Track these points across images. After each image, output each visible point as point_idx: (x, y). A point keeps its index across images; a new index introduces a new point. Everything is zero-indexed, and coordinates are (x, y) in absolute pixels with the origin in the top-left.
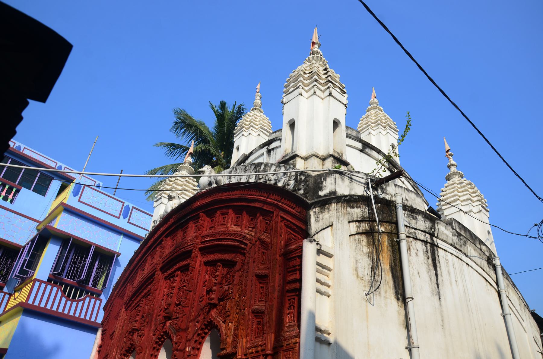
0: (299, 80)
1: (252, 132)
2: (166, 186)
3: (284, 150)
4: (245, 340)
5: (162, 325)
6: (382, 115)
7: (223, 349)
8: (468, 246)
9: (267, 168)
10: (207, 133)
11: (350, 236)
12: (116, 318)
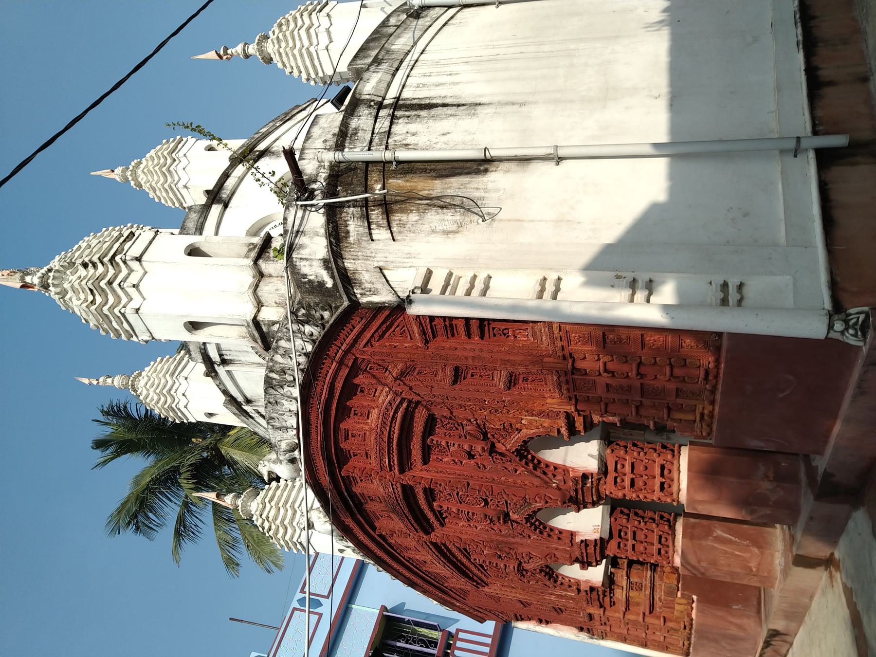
0: (107, 313)
1: (181, 391)
2: (280, 536)
3: (242, 339)
4: (549, 401)
5: (515, 525)
6: (150, 163)
7: (559, 431)
8: (393, 47)
9: (277, 367)
10: (152, 471)
11: (394, 240)
12: (498, 600)
